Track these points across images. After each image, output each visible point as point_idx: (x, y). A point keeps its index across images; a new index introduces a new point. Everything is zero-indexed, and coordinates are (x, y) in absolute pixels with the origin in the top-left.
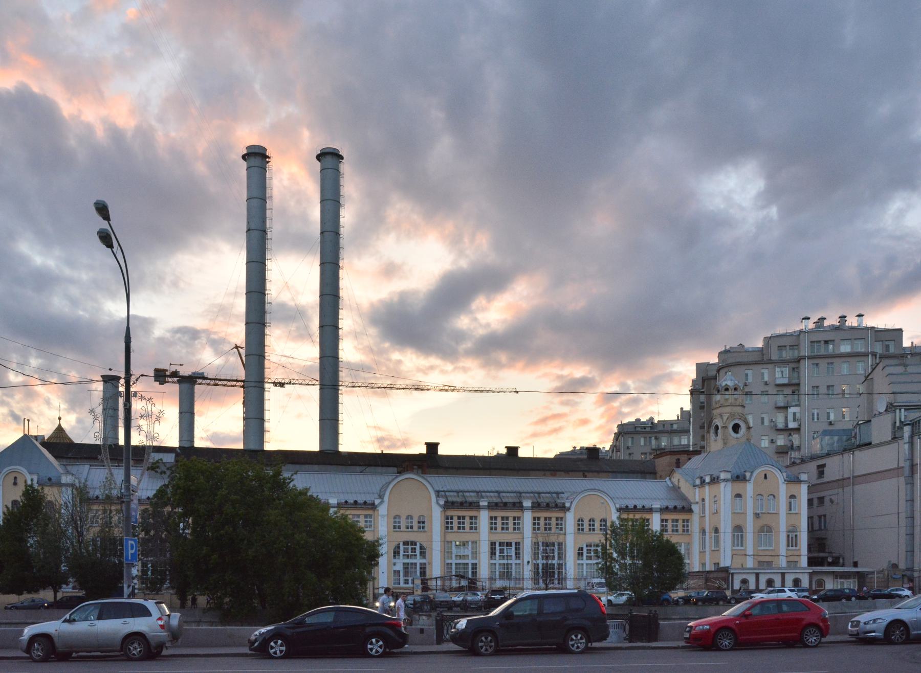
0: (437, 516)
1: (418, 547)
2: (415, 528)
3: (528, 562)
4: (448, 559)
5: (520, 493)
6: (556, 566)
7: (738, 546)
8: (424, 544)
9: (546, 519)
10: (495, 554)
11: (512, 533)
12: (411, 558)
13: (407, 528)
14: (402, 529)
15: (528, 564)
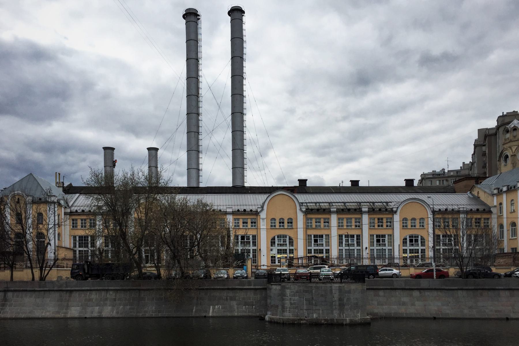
0: (300, 218)
1: (419, 238)
2: (277, 227)
3: (366, 248)
4: (309, 246)
5: (360, 203)
6: (348, 248)
7: (514, 236)
8: (292, 236)
9: (379, 219)
10: (342, 243)
11: (385, 229)
12: (283, 246)
13: (412, 226)
14: (416, 227)
15: (366, 250)
